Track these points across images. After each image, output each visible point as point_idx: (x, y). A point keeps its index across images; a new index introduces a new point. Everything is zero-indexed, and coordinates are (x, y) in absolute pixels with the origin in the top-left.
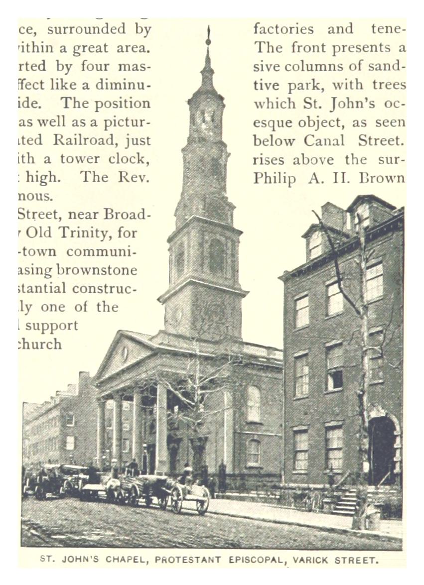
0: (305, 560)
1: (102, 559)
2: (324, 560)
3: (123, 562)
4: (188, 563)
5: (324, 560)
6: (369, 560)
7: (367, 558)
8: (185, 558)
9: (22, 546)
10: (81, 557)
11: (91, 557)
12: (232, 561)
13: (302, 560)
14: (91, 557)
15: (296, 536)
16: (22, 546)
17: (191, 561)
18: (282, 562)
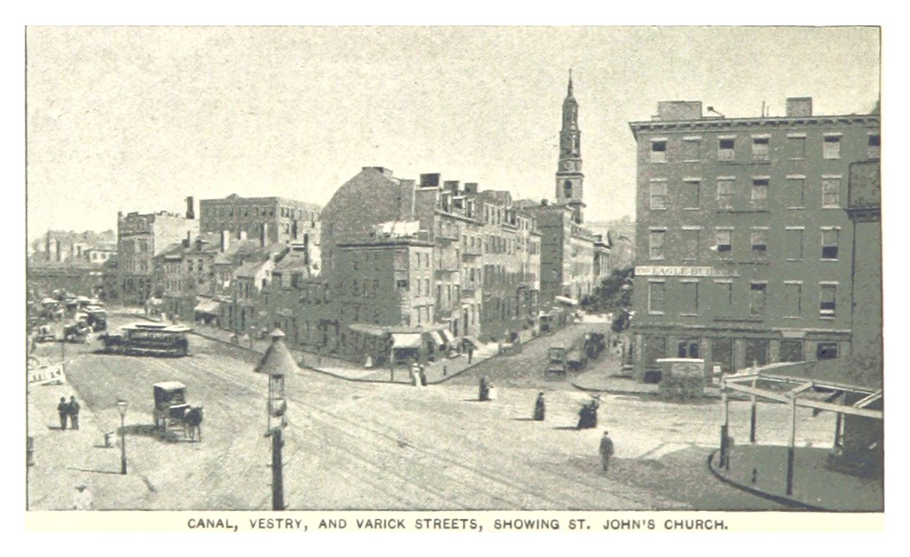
0: (373, 524)
1: (659, 523)
2: (400, 524)
3: (220, 526)
4: (267, 528)
5: (400, 524)
6: (460, 524)
7: (457, 520)
8: (446, 522)
9: (882, 510)
10: (682, 521)
11: (644, 521)
12: (262, 525)
13: (369, 524)
14: (644, 521)
15: (232, 480)
16: (882, 510)
17: (270, 525)
18: (231, 527)
